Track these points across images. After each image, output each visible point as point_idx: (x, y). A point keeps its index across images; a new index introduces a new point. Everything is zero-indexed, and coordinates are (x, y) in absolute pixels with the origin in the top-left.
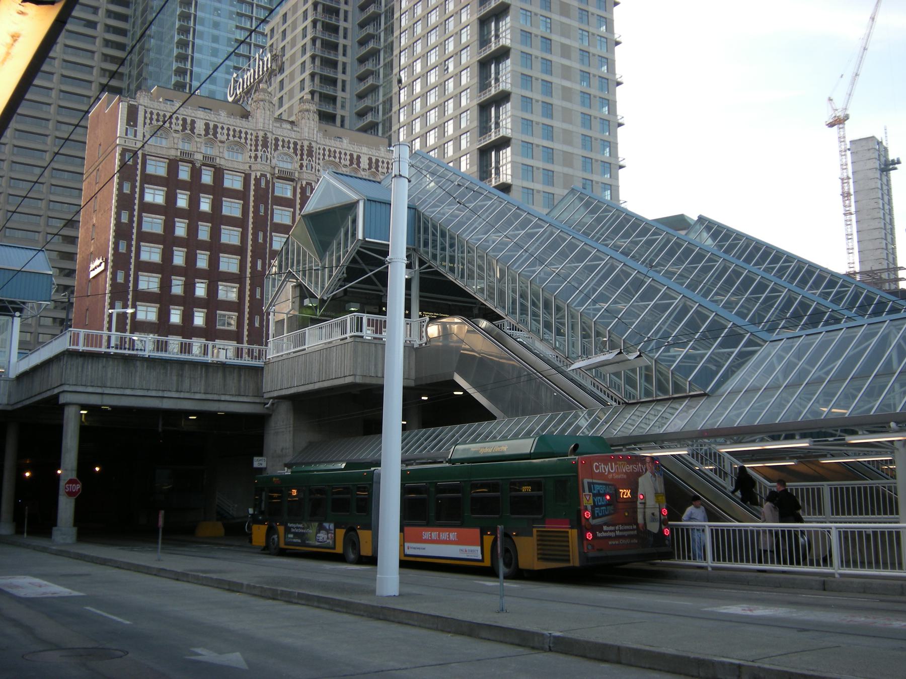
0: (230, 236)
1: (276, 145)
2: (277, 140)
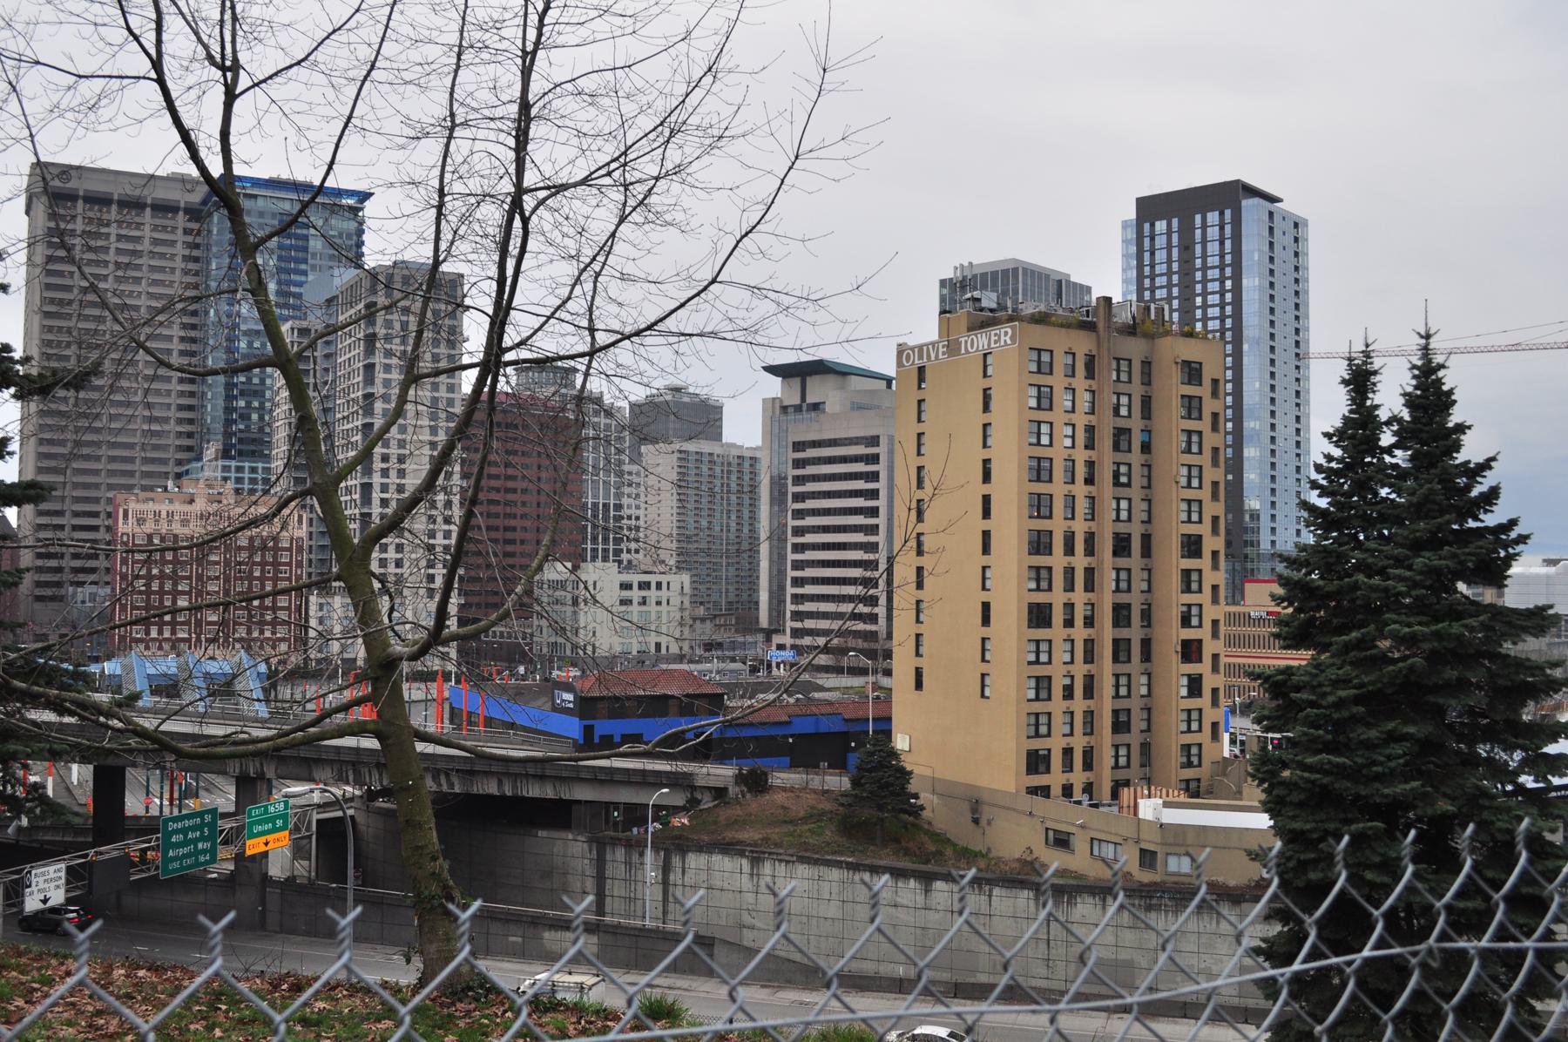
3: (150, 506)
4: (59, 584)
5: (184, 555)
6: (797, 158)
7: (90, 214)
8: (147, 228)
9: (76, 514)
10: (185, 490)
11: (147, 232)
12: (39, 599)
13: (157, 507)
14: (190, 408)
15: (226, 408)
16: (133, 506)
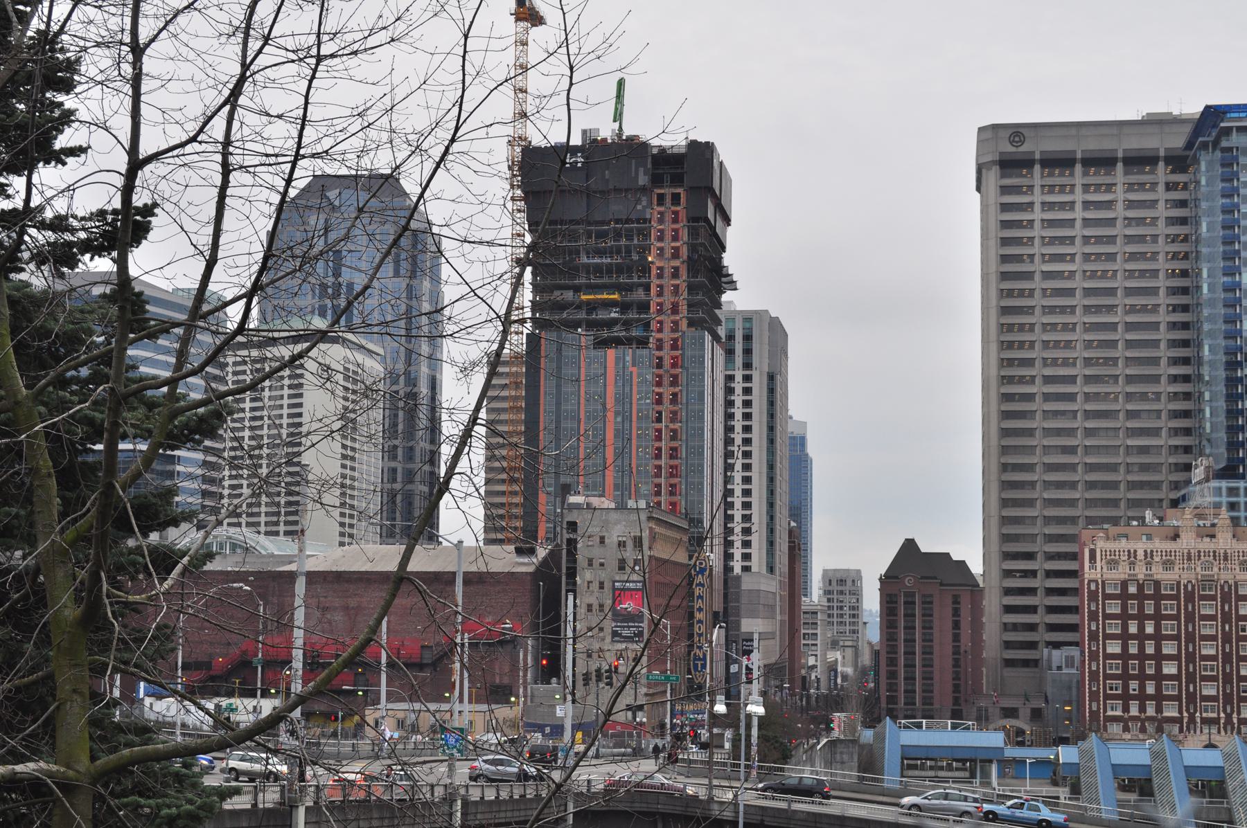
0: (1170, 669)
1: (1199, 556)
2: (1199, 552)
3: (1123, 544)
4: (1032, 645)
5: (1169, 608)
6: (571, 68)
7: (1050, 181)
8: (1119, 188)
9: (1051, 557)
10: (1167, 523)
11: (1120, 194)
12: (1009, 663)
13: (1131, 546)
14: (1186, 414)
15: (1229, 412)
16: (1101, 545)
